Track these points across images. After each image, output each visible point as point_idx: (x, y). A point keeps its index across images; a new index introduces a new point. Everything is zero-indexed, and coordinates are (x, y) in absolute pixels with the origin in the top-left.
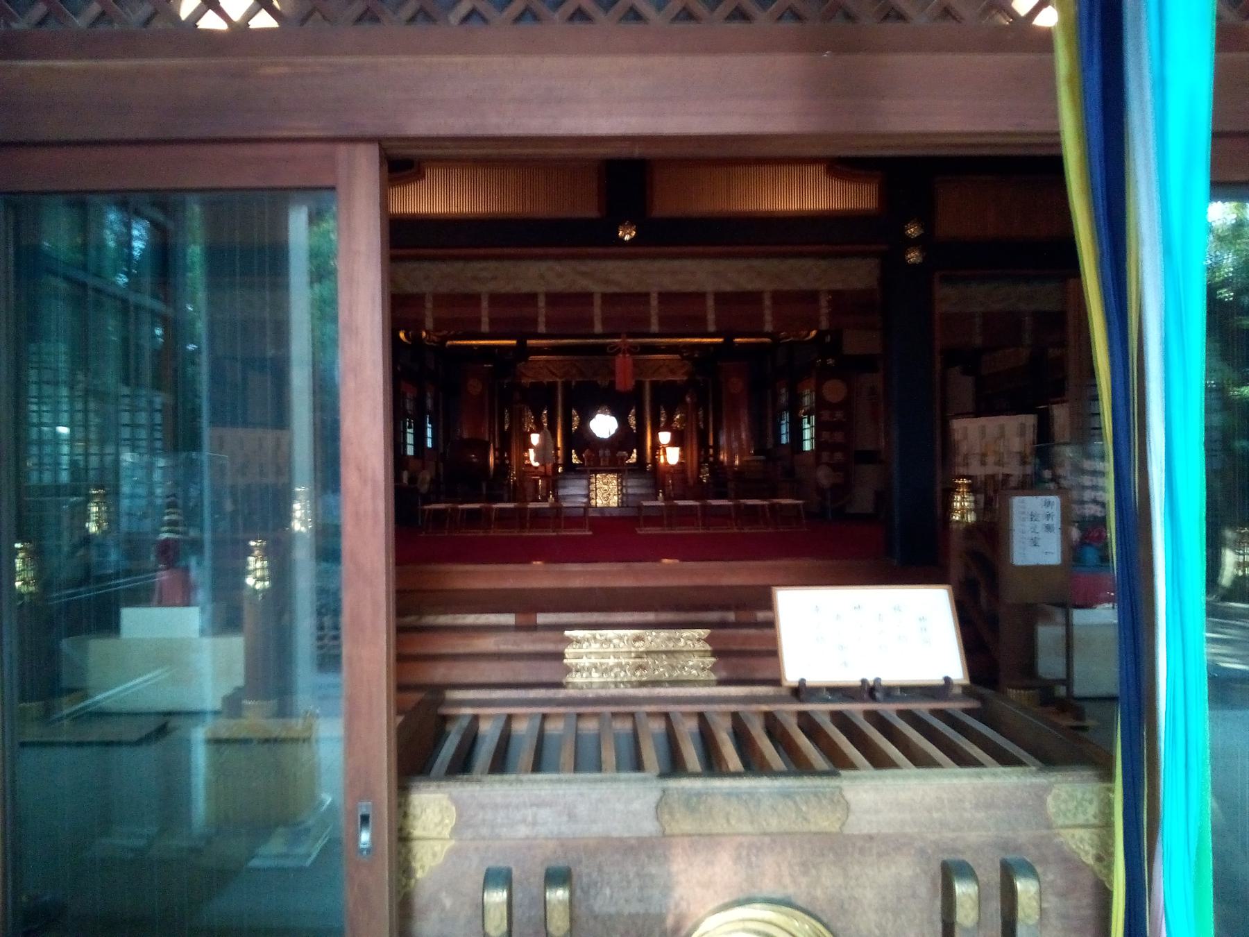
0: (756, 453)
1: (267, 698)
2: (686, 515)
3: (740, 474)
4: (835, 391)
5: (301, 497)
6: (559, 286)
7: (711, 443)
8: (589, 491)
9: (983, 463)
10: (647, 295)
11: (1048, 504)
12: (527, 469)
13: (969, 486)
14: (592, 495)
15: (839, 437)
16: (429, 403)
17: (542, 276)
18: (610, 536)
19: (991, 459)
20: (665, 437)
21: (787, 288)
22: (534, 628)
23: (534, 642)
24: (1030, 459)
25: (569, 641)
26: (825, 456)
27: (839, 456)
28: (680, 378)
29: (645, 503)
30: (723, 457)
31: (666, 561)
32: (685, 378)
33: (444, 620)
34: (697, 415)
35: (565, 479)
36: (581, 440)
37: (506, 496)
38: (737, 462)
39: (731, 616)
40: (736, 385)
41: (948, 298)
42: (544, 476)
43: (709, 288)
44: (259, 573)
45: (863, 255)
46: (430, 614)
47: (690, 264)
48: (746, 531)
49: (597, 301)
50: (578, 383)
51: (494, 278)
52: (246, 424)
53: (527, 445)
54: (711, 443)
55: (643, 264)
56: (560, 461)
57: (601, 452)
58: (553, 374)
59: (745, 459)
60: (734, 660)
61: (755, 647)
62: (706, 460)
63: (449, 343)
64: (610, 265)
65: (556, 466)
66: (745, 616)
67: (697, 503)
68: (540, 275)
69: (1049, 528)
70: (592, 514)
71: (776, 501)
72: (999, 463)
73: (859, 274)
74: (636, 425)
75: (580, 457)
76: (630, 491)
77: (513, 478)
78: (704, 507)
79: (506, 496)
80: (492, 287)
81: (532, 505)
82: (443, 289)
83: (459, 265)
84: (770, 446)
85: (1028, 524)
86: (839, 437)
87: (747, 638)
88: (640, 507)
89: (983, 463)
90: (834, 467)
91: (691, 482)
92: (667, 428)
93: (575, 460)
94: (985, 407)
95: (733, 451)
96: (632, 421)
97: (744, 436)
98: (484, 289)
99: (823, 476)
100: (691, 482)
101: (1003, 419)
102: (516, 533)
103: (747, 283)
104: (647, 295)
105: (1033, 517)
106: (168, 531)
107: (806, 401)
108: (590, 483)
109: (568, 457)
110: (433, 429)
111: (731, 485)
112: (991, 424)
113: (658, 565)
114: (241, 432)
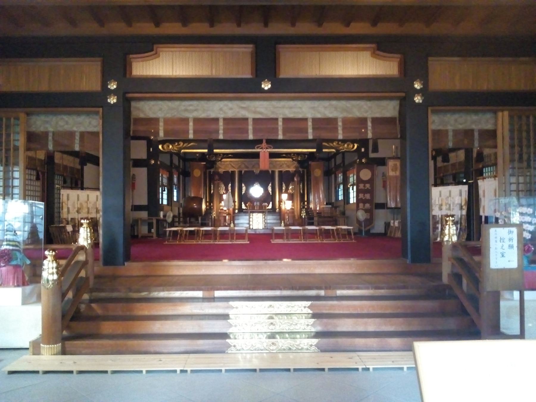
0: (327, 204)
1: (56, 343)
2: (295, 234)
3: (319, 214)
4: (366, 174)
5: (85, 225)
6: (230, 114)
7: (306, 200)
8: (250, 221)
9: (441, 209)
10: (277, 119)
11: (510, 232)
12: (222, 211)
13: (453, 221)
14: (251, 223)
15: (368, 196)
16: (175, 180)
17: (221, 109)
18: (259, 246)
19: (444, 207)
20: (285, 196)
21: (350, 116)
22: (213, 299)
23: (212, 308)
24: (464, 207)
25: (232, 308)
26: (361, 205)
27: (368, 206)
28: (292, 169)
29: (276, 228)
30: (312, 206)
31: (285, 260)
32: (294, 170)
33: (162, 294)
34: (300, 186)
35: (238, 216)
36: (244, 198)
37: (210, 224)
38: (318, 209)
39: (322, 293)
40: (318, 172)
41: (436, 122)
42: (229, 214)
43: (309, 116)
44: (51, 271)
45: (391, 99)
46: (155, 291)
47: (299, 103)
48: (325, 242)
49: (250, 122)
50: (245, 171)
51: (196, 110)
52: (82, 188)
53: (221, 200)
54: (306, 200)
55: (274, 103)
56: (237, 207)
57: (255, 204)
58: (233, 167)
59: (322, 207)
60: (325, 320)
61: (337, 312)
62: (304, 207)
63: (183, 151)
64: (257, 103)
65: (234, 209)
66: (330, 293)
67: (301, 228)
68: (221, 109)
69: (511, 247)
70: (249, 232)
71: (338, 227)
72: (449, 209)
73: (389, 109)
74: (272, 191)
75: (246, 206)
76: (268, 221)
77: (214, 214)
78: (304, 230)
79: (210, 224)
80: (196, 114)
81: (220, 229)
82: (169, 116)
83: (177, 103)
84: (333, 200)
85: (499, 244)
86: (368, 196)
87: (332, 306)
88: (273, 230)
89: (441, 209)
90: (366, 211)
91: (297, 218)
92: (286, 192)
93: (244, 207)
94: (440, 182)
95: (317, 202)
96: (270, 189)
97: (321, 196)
98: (191, 116)
99: (361, 215)
100: (297, 218)
101: (450, 188)
102: (212, 242)
103: (330, 114)
104: (277, 119)
105: (502, 240)
106: (7, 245)
107: (351, 180)
108: (250, 218)
109: (240, 205)
110: (177, 192)
111: (316, 219)
112: (444, 190)
113: (281, 262)
114: (79, 192)
